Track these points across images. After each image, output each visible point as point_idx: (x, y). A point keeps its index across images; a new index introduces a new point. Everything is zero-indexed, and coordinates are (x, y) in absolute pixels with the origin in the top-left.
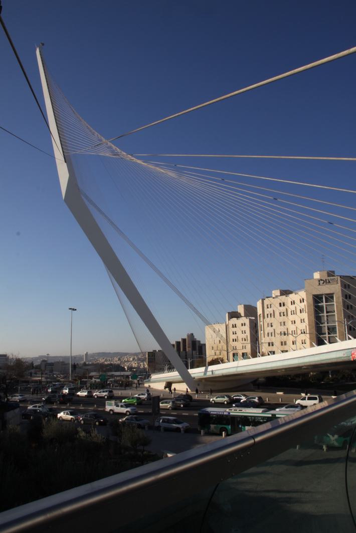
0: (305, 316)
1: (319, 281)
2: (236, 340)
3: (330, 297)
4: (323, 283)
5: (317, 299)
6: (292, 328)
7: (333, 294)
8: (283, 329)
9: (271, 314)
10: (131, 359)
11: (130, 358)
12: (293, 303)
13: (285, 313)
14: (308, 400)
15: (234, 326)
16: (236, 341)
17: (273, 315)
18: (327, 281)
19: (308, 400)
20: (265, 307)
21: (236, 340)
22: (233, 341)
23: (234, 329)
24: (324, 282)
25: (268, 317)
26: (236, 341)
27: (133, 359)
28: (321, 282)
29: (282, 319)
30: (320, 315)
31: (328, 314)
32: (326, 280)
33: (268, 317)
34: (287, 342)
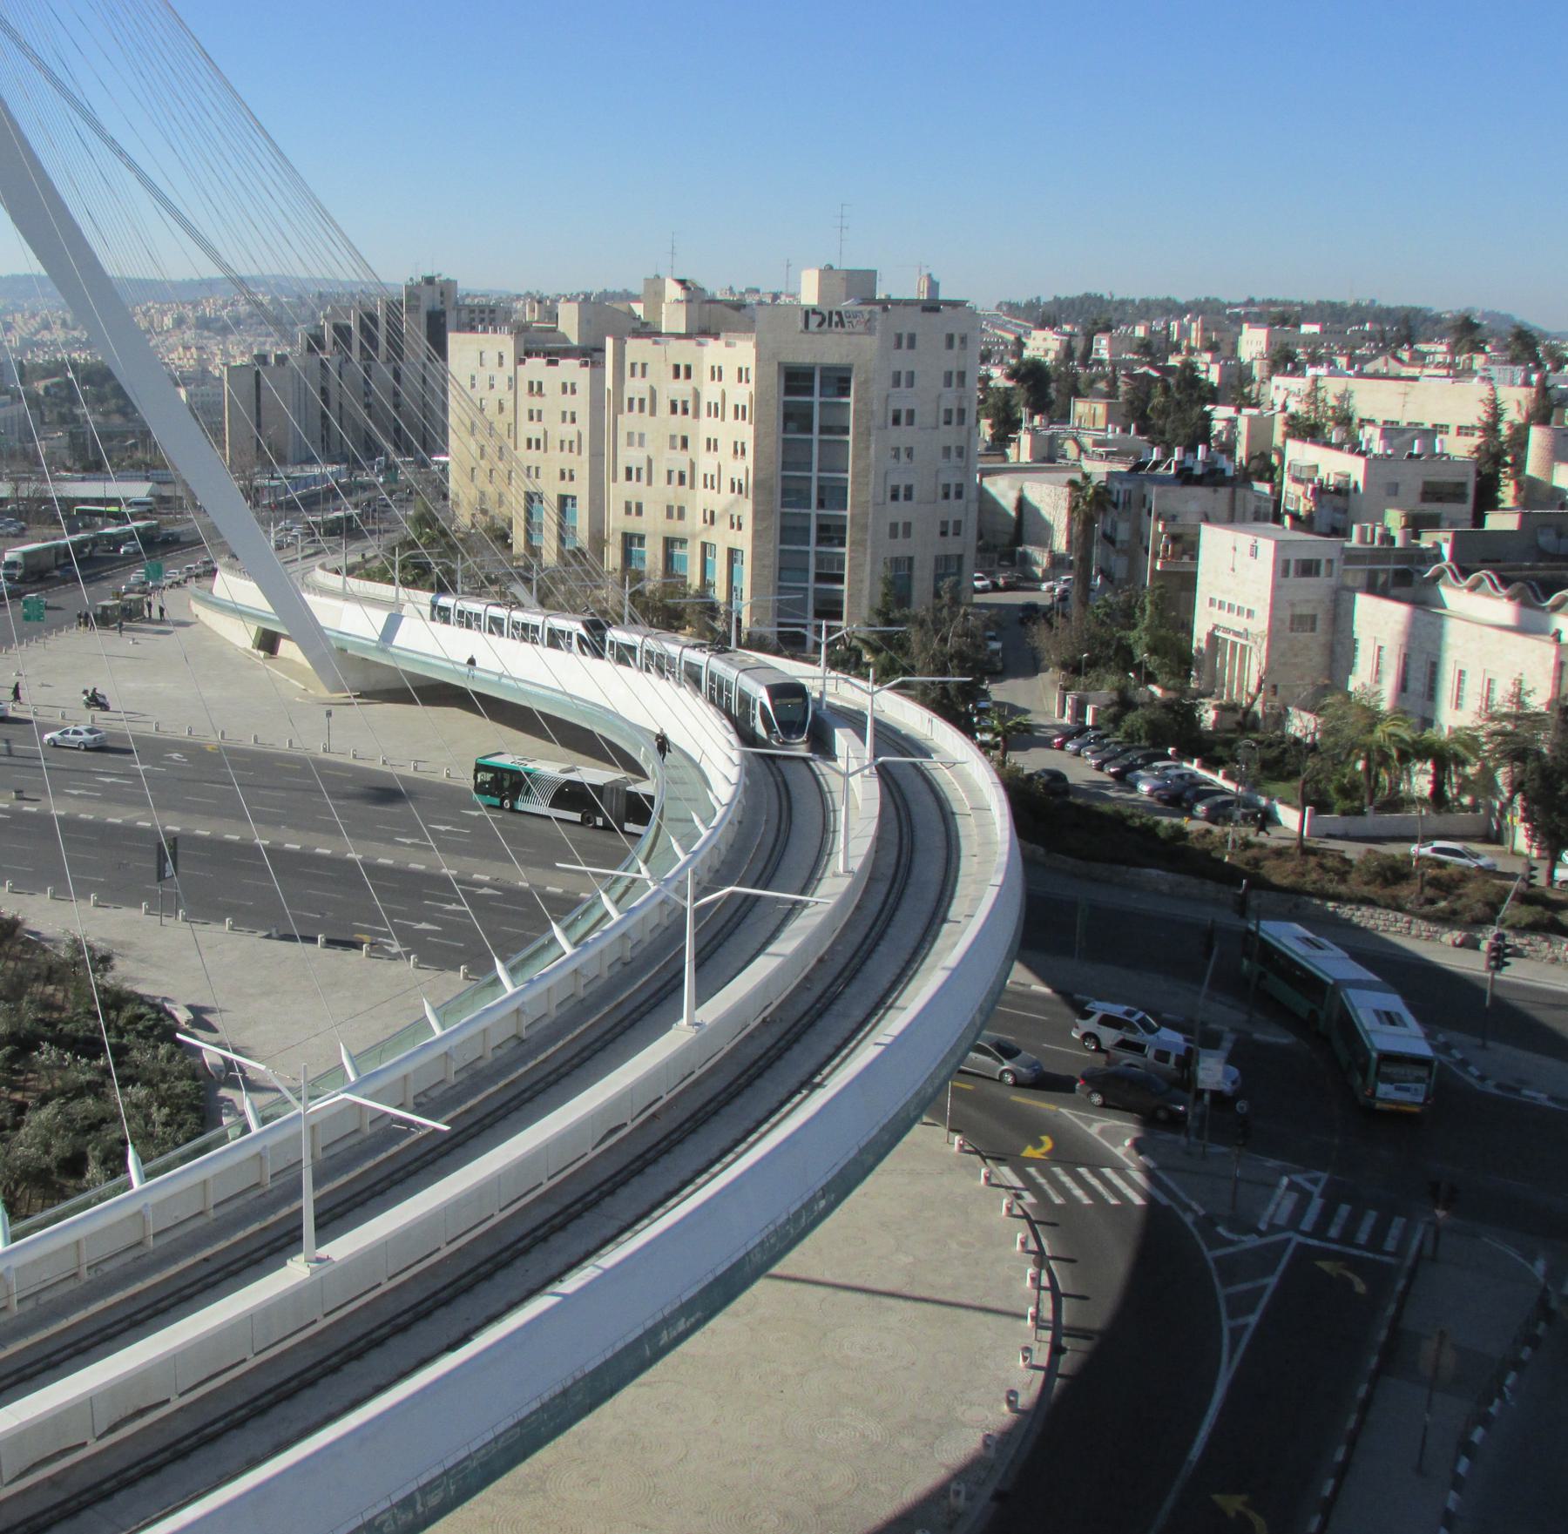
0: (746, 432)
1: (807, 313)
2: (538, 441)
3: (839, 380)
4: (820, 325)
5: (796, 379)
6: (706, 464)
7: (848, 369)
8: (679, 461)
9: (642, 401)
10: (168, 321)
11: (164, 313)
12: (717, 374)
13: (690, 407)
14: (1318, 562)
15: (536, 389)
16: (538, 447)
17: (648, 404)
18: (835, 318)
19: (1318, 562)
20: (622, 439)
21: (538, 441)
22: (529, 446)
23: (536, 403)
24: (823, 320)
25: (633, 375)
26: (538, 447)
27: (180, 322)
28: (814, 320)
29: (679, 424)
30: (498, 964)
31: (826, 437)
32: (831, 313)
33: (633, 375)
34: (688, 511)
